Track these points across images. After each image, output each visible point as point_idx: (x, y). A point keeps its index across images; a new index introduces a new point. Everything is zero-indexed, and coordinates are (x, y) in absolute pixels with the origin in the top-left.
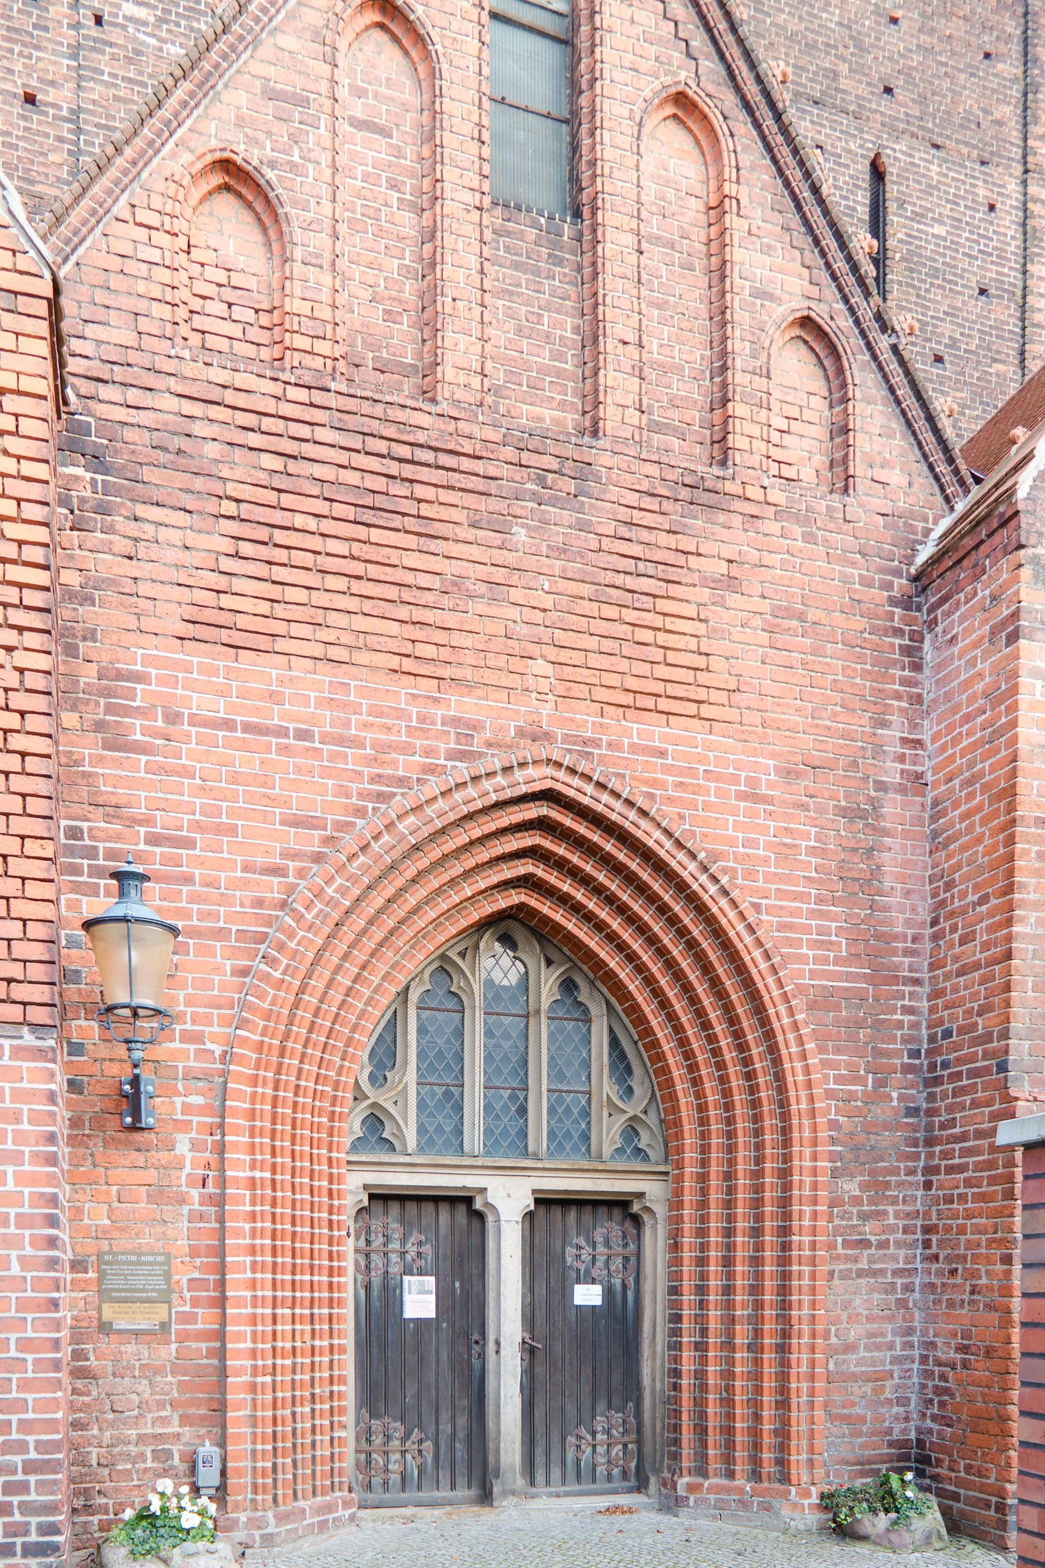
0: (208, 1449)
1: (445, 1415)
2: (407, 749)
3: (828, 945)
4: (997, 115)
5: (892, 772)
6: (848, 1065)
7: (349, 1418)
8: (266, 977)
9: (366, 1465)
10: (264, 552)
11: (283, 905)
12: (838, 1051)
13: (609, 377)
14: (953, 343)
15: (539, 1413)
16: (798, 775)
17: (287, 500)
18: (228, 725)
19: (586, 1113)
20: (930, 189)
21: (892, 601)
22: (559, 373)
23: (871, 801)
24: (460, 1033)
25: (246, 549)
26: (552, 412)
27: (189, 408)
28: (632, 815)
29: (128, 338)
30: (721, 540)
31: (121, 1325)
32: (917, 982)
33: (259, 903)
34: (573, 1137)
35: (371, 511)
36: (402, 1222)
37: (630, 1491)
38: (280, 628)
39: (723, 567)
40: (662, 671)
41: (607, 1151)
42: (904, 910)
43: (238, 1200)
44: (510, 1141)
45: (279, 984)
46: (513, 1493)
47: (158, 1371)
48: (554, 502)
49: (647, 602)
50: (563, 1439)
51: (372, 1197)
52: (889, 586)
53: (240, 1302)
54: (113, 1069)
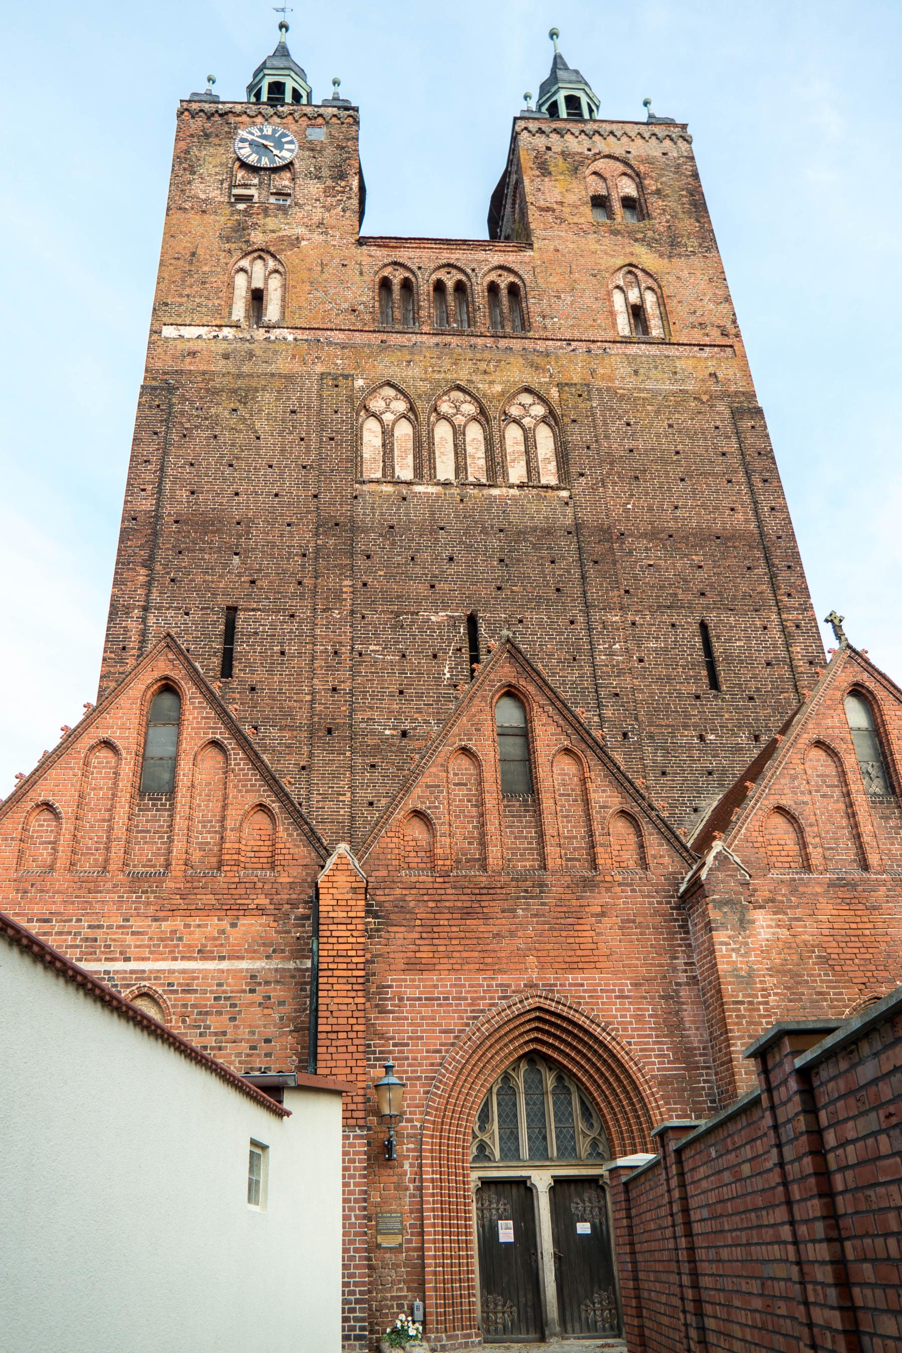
0: (418, 1303)
1: (521, 1293)
2: (484, 998)
3: (664, 1056)
4: (759, 590)
5: (682, 978)
6: (681, 1110)
7: (477, 1291)
8: (435, 1094)
9: (486, 1320)
10: (430, 935)
11: (441, 1064)
12: (675, 1104)
13: (549, 849)
14: (758, 690)
15: (566, 1292)
16: (641, 985)
17: (437, 916)
18: (420, 999)
19: (573, 1137)
20: (731, 628)
21: (672, 908)
22: (531, 849)
23: (674, 991)
24: (515, 1105)
25: (424, 935)
26: (528, 863)
27: (404, 892)
28: (572, 1012)
29: (385, 873)
30: (597, 901)
31: (384, 1245)
32: (708, 1068)
33: (432, 1064)
34: (567, 1151)
35: (467, 913)
36: (496, 1194)
37: (615, 1337)
38: (437, 961)
39: (599, 909)
40: (579, 953)
41: (584, 1155)
42: (695, 1036)
43: (428, 1188)
44: (540, 1153)
45: (440, 1096)
46: (555, 1335)
47: (398, 1266)
48: (532, 898)
49: (571, 927)
50: (579, 1306)
51: (482, 1183)
52: (669, 903)
53: (429, 1234)
54: (381, 1136)
